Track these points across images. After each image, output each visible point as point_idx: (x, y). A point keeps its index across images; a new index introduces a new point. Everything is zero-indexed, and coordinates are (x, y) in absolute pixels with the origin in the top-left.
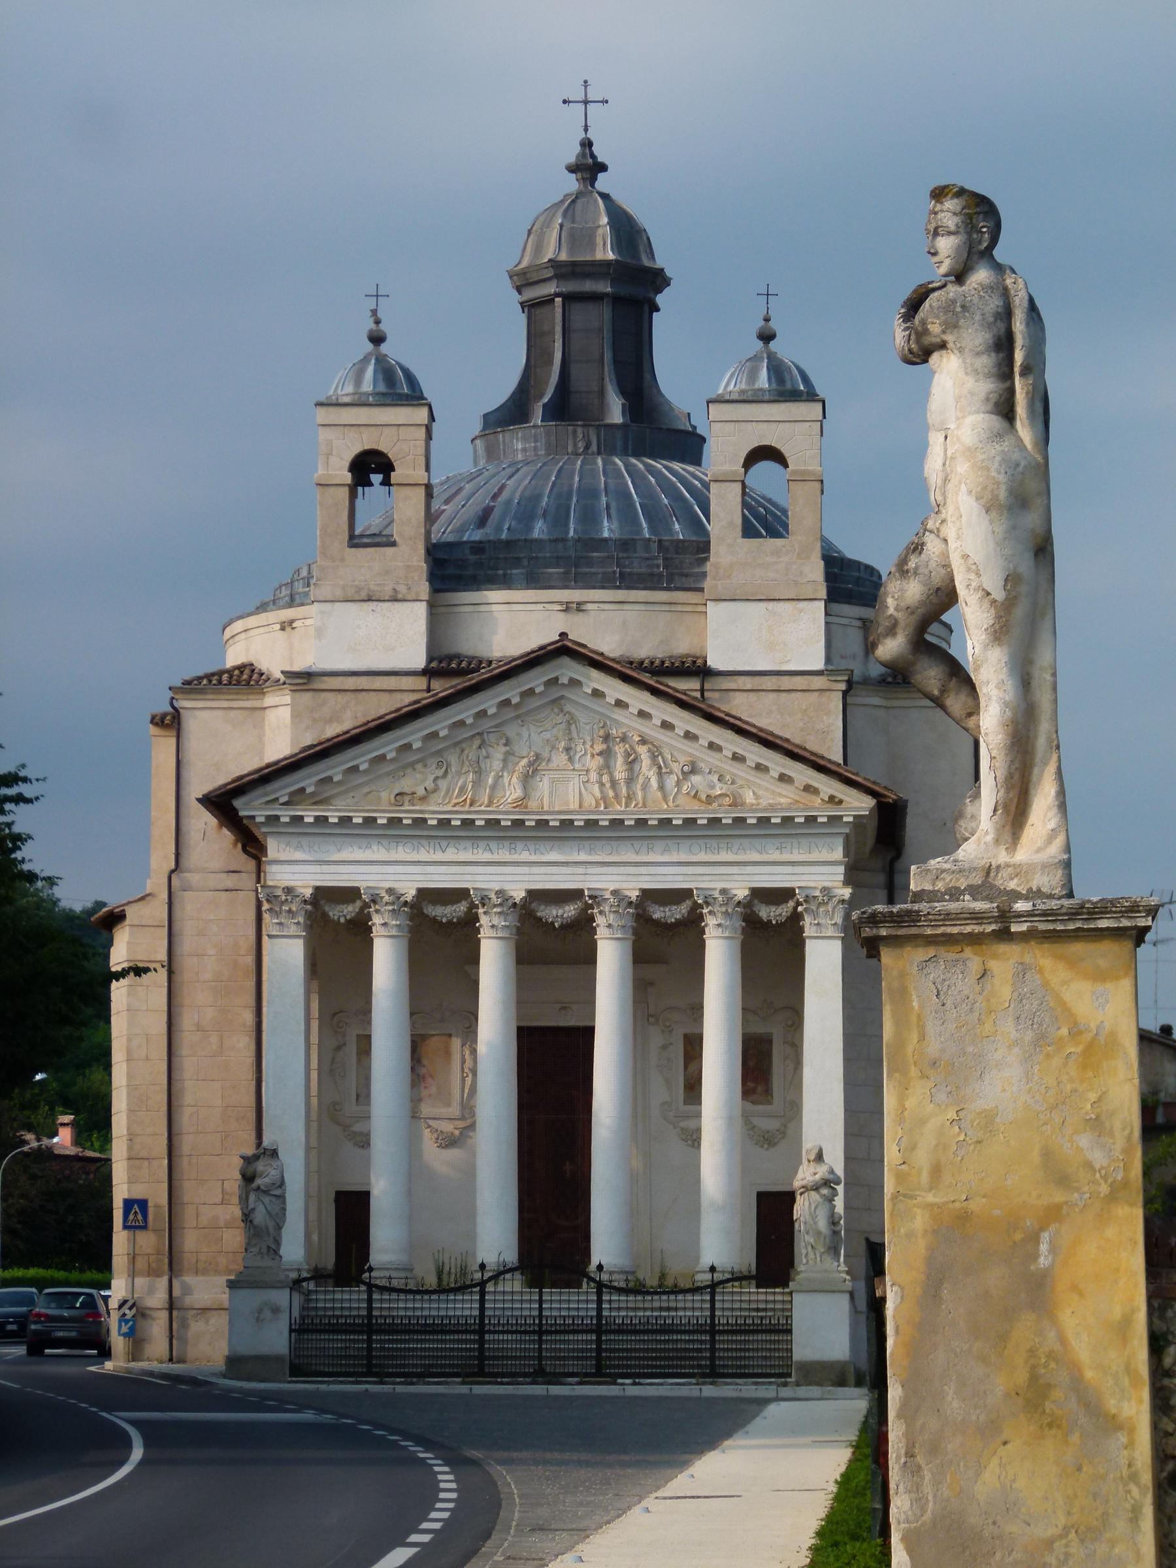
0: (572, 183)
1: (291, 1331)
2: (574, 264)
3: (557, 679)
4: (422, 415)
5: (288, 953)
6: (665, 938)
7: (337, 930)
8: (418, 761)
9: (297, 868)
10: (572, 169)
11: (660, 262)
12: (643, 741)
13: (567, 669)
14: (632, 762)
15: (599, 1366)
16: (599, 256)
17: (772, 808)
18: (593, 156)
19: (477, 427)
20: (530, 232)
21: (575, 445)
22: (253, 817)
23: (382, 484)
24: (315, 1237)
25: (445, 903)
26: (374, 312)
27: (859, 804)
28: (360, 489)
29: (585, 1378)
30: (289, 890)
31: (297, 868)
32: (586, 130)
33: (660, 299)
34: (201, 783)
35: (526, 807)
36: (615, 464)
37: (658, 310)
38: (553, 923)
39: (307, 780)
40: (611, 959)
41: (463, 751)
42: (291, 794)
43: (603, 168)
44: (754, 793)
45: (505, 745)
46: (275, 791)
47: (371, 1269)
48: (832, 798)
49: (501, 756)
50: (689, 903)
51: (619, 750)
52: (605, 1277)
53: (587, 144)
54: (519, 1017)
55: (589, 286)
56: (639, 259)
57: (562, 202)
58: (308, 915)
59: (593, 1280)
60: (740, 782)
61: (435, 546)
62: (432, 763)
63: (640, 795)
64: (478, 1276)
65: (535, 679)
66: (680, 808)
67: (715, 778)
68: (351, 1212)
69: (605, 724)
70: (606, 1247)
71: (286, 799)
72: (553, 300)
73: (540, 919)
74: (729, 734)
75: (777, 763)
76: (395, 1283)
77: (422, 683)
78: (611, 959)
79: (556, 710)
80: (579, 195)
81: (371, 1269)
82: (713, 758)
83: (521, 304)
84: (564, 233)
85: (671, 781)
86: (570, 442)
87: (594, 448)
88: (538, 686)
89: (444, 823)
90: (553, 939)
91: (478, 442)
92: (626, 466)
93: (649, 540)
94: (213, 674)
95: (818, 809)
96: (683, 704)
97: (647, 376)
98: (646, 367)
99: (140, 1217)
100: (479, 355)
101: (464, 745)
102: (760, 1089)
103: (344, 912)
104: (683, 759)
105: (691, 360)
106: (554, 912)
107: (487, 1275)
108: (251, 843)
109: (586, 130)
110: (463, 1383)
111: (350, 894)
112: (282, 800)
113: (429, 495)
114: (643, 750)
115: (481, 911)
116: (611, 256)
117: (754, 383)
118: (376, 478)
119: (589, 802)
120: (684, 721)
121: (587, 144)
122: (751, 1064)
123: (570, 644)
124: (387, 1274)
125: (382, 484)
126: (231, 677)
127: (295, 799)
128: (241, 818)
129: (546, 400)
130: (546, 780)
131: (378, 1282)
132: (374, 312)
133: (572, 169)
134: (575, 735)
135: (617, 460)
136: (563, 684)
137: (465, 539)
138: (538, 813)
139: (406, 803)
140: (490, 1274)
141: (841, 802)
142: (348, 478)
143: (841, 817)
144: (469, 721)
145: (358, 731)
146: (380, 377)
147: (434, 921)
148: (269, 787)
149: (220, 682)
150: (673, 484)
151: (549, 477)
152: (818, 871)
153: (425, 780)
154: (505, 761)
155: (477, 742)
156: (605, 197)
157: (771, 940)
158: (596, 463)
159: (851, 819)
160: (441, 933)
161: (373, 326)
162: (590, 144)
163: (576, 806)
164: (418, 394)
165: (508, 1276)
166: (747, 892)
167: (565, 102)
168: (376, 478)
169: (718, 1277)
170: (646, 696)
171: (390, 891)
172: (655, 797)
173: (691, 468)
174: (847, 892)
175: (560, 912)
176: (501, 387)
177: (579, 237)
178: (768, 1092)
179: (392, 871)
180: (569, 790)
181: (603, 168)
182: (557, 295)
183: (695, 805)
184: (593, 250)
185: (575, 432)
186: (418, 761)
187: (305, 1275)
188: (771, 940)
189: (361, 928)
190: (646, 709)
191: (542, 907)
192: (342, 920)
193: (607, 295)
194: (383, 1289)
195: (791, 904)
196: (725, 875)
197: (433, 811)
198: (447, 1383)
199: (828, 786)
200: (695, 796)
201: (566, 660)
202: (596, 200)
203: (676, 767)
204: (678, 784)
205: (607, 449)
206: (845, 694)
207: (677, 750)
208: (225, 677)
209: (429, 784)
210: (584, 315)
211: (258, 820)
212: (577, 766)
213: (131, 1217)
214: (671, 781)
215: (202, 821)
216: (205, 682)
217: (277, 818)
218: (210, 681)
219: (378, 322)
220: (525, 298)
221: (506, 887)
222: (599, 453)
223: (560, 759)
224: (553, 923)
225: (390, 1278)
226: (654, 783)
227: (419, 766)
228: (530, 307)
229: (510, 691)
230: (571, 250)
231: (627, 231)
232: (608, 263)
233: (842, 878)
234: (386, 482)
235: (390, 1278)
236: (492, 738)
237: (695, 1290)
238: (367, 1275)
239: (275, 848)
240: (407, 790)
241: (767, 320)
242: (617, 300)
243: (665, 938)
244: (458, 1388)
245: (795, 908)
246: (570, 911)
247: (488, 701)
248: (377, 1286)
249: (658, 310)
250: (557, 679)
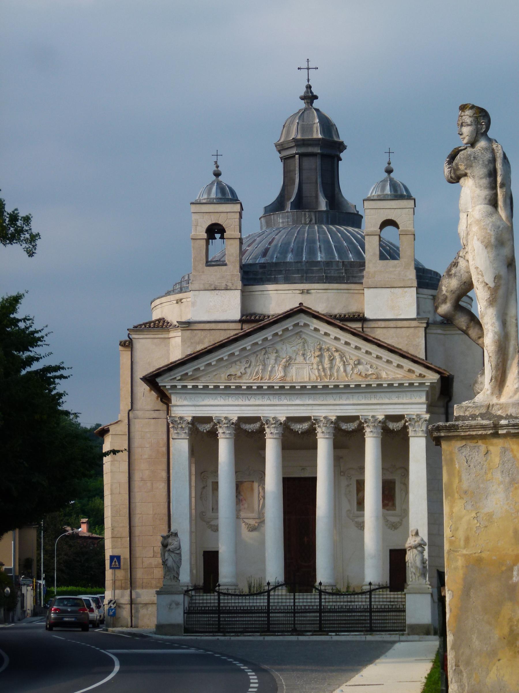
0: (302, 105)
1: (184, 613)
2: (303, 140)
3: (298, 323)
4: (237, 208)
5: (181, 446)
6: (347, 437)
7: (202, 436)
8: (237, 361)
9: (185, 408)
10: (302, 98)
11: (342, 139)
12: (337, 351)
13: (303, 319)
14: (332, 360)
15: (320, 627)
16: (315, 136)
17: (394, 379)
18: (311, 92)
19: (262, 213)
20: (284, 126)
21: (305, 220)
22: (165, 386)
23: (220, 238)
24: (194, 572)
25: (250, 423)
26: (216, 162)
27: (433, 377)
28: (211, 241)
29: (315, 633)
30: (181, 418)
31: (185, 408)
32: (308, 81)
33: (342, 155)
34: (142, 371)
35: (285, 380)
36: (323, 228)
37: (341, 160)
38: (298, 431)
39: (189, 369)
40: (324, 447)
41: (257, 356)
42: (182, 376)
43: (316, 97)
44: (386, 373)
45: (276, 353)
46: (174, 375)
47: (219, 586)
48: (420, 375)
49: (274, 358)
50: (358, 422)
51: (326, 354)
52: (323, 588)
53: (309, 87)
54: (284, 473)
55: (310, 150)
56: (332, 137)
57: (298, 113)
58: (190, 429)
59: (317, 589)
60: (379, 368)
61: (244, 265)
62: (244, 361)
63: (335, 374)
64: (266, 588)
65: (289, 324)
66: (354, 380)
67: (368, 366)
68: (210, 560)
69: (320, 343)
70: (323, 574)
71: (179, 378)
72: (295, 156)
73: (292, 430)
74: (375, 347)
75: (396, 359)
76: (230, 592)
77: (239, 326)
78: (324, 447)
79: (298, 337)
80: (305, 110)
81: (219, 586)
82: (368, 358)
83: (281, 158)
84: (299, 127)
85: (349, 368)
86: (303, 219)
87: (314, 221)
88: (290, 327)
89: (249, 388)
90: (298, 439)
91: (262, 219)
92: (328, 229)
93: (338, 261)
94: (147, 323)
95: (414, 380)
96: (354, 334)
97: (337, 189)
98: (336, 185)
99: (117, 563)
100: (262, 181)
101: (258, 353)
102: (390, 504)
103: (206, 427)
104: (354, 358)
105: (356, 181)
106: (298, 427)
107: (271, 588)
108: (164, 397)
109: (308, 81)
110: (261, 635)
111: (208, 420)
112: (178, 378)
113: (241, 243)
114: (336, 355)
115: (266, 426)
116: (320, 136)
117: (384, 191)
118: (218, 236)
119: (313, 377)
120: (355, 341)
121: (309, 87)
122: (386, 493)
123: (304, 308)
124: (226, 587)
125: (220, 238)
126: (155, 324)
127: (183, 378)
128: (160, 387)
129: (292, 200)
130: (294, 368)
131: (222, 591)
132: (216, 162)
133: (302, 98)
134: (306, 348)
135: (324, 227)
136: (301, 326)
137: (257, 262)
138: (291, 383)
139: (233, 379)
140: (272, 587)
141: (424, 376)
142: (205, 236)
143: (424, 383)
144: (260, 342)
145: (211, 347)
146: (219, 191)
147: (246, 431)
148: (172, 373)
149: (150, 327)
150: (349, 237)
151: (294, 235)
152: (415, 407)
153: (240, 369)
154: (276, 360)
155: (263, 352)
156: (317, 110)
157: (394, 438)
158: (315, 228)
159: (429, 384)
160: (249, 436)
161: (215, 169)
162: (310, 87)
163: (308, 379)
164: (236, 198)
165: (280, 588)
166: (383, 417)
167: (299, 69)
168: (218, 236)
169: (373, 587)
170: (338, 330)
171: (226, 418)
172: (342, 375)
173: (356, 230)
174: (427, 416)
175: (301, 426)
176: (272, 195)
177: (306, 128)
178: (394, 505)
179: (226, 409)
180: (304, 372)
181: (316, 97)
182: (296, 154)
183: (360, 379)
184: (312, 134)
185: (305, 214)
186: (237, 361)
187: (190, 588)
188: (394, 438)
189: (213, 435)
190: (338, 336)
191: (293, 424)
192: (205, 431)
193: (318, 153)
194: (225, 594)
195: (403, 422)
196: (374, 409)
197: (245, 382)
198: (253, 635)
199: (419, 370)
200: (360, 374)
201: (302, 315)
202: (313, 112)
203: (351, 362)
204: (352, 369)
205: (319, 222)
206: (426, 328)
207: (352, 354)
208: (152, 324)
209: (243, 370)
210: (308, 163)
211: (167, 387)
212: (308, 362)
213: (113, 563)
214: (349, 368)
215: (143, 388)
216: (143, 326)
217: (176, 386)
218: (145, 326)
219: (217, 167)
220: (282, 156)
221: (277, 415)
222: (316, 223)
223: (300, 359)
224: (298, 431)
225: (228, 589)
226: (342, 369)
227: (238, 363)
228: (285, 159)
229: (278, 329)
230: (302, 136)
231: (327, 125)
232: (319, 140)
233: (425, 410)
234: (222, 237)
235: (228, 589)
236: (270, 350)
237: (363, 593)
238: (218, 588)
239: (175, 400)
240: (233, 373)
241: (389, 164)
242: (323, 156)
243: (347, 437)
244: (257, 638)
245: (405, 424)
246: (305, 426)
247: (268, 334)
248: (222, 593)
249: (341, 160)
250: (298, 323)
